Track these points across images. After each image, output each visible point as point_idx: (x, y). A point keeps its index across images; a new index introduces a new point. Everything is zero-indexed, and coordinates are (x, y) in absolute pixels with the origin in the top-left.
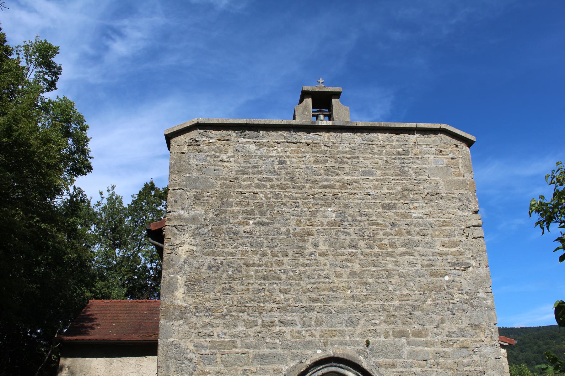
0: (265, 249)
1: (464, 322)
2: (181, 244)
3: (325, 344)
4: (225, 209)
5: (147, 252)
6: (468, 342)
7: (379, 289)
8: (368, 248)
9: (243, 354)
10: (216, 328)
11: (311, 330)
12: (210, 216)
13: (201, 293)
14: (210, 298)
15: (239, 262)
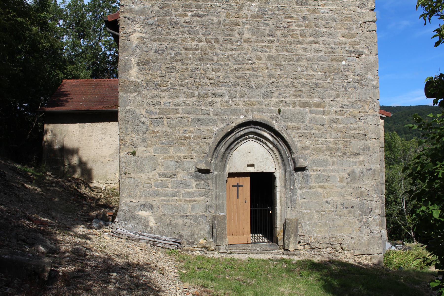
0: (200, 36)
1: (354, 97)
2: (133, 33)
3: (247, 111)
4: (168, 3)
5: (106, 41)
6: (356, 112)
7: (290, 70)
8: (283, 37)
9: (184, 118)
10: (162, 99)
11: (236, 100)
12: (156, 9)
13: (150, 71)
14: (158, 75)
15: (180, 46)
